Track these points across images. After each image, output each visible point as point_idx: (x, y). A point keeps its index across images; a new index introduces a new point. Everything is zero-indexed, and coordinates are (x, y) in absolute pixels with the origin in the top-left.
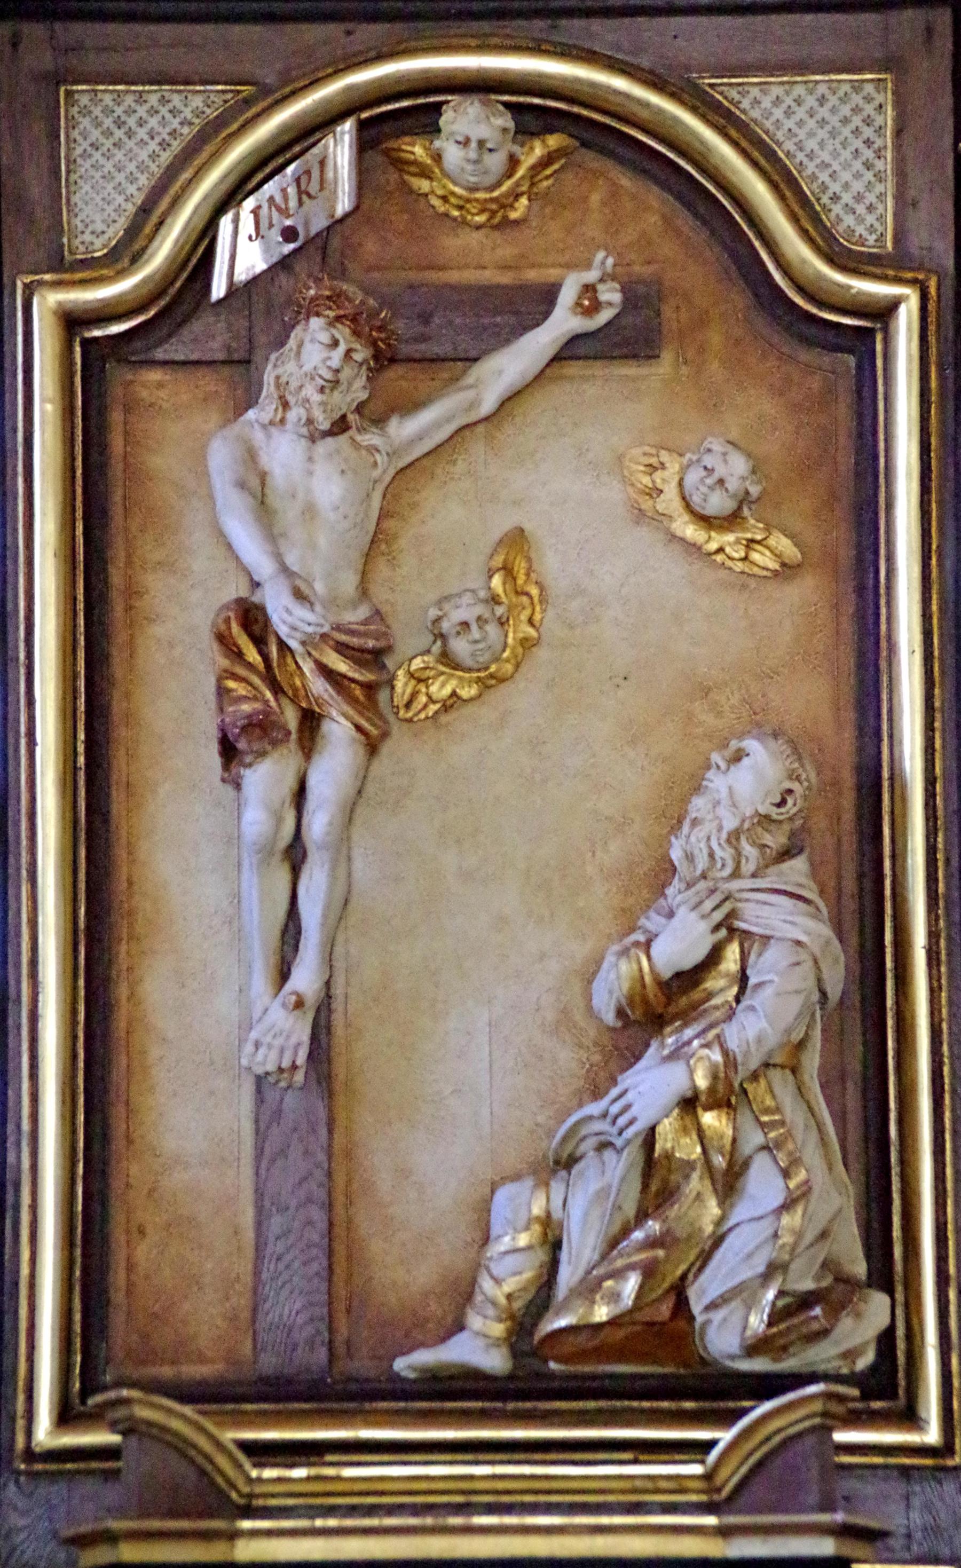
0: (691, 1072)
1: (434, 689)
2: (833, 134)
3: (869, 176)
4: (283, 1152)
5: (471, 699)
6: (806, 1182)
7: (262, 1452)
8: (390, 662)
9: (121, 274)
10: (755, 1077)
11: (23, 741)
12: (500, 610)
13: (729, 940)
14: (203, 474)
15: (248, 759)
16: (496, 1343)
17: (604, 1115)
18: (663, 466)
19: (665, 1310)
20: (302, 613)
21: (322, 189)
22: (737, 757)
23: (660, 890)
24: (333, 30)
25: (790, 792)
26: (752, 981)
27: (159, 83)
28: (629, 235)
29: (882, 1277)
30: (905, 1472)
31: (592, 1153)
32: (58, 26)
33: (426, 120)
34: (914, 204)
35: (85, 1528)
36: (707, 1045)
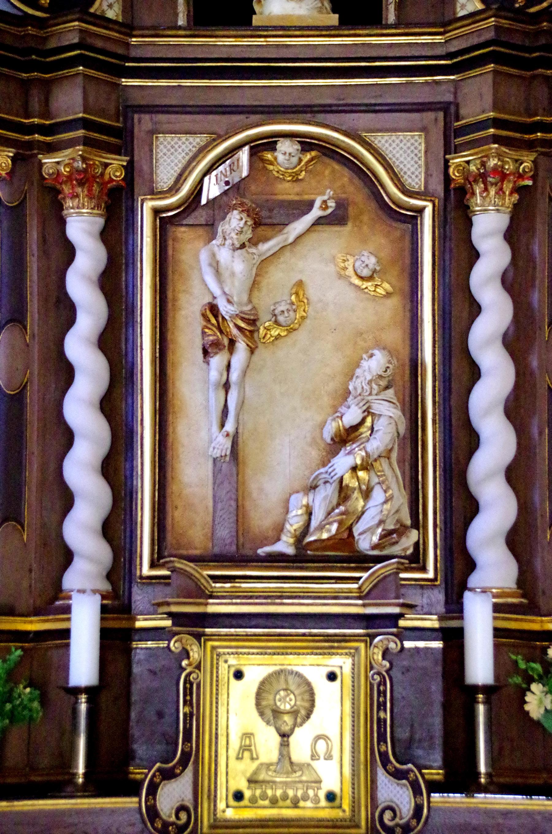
0: (355, 458)
1: (272, 333)
2: (405, 152)
3: (416, 166)
4: (222, 483)
5: (285, 336)
6: (392, 494)
7: (216, 579)
8: (258, 323)
9: (172, 196)
10: (375, 460)
11: (139, 349)
12: (294, 307)
13: (368, 416)
14: (198, 261)
15: (212, 355)
16: (291, 545)
17: (326, 472)
18: (348, 260)
19: (345, 535)
20: (230, 307)
21: (238, 168)
22: (372, 356)
23: (345, 399)
24: (242, 117)
25: (388, 367)
26: (375, 429)
27: (186, 134)
28: (338, 184)
29: (416, 525)
30: (422, 587)
31: (322, 484)
32: (153, 115)
33: (272, 147)
34: (431, 175)
35: (161, 600)
36: (360, 450)
